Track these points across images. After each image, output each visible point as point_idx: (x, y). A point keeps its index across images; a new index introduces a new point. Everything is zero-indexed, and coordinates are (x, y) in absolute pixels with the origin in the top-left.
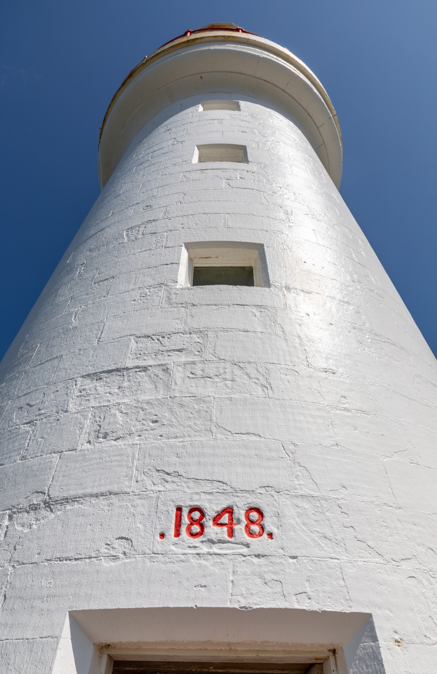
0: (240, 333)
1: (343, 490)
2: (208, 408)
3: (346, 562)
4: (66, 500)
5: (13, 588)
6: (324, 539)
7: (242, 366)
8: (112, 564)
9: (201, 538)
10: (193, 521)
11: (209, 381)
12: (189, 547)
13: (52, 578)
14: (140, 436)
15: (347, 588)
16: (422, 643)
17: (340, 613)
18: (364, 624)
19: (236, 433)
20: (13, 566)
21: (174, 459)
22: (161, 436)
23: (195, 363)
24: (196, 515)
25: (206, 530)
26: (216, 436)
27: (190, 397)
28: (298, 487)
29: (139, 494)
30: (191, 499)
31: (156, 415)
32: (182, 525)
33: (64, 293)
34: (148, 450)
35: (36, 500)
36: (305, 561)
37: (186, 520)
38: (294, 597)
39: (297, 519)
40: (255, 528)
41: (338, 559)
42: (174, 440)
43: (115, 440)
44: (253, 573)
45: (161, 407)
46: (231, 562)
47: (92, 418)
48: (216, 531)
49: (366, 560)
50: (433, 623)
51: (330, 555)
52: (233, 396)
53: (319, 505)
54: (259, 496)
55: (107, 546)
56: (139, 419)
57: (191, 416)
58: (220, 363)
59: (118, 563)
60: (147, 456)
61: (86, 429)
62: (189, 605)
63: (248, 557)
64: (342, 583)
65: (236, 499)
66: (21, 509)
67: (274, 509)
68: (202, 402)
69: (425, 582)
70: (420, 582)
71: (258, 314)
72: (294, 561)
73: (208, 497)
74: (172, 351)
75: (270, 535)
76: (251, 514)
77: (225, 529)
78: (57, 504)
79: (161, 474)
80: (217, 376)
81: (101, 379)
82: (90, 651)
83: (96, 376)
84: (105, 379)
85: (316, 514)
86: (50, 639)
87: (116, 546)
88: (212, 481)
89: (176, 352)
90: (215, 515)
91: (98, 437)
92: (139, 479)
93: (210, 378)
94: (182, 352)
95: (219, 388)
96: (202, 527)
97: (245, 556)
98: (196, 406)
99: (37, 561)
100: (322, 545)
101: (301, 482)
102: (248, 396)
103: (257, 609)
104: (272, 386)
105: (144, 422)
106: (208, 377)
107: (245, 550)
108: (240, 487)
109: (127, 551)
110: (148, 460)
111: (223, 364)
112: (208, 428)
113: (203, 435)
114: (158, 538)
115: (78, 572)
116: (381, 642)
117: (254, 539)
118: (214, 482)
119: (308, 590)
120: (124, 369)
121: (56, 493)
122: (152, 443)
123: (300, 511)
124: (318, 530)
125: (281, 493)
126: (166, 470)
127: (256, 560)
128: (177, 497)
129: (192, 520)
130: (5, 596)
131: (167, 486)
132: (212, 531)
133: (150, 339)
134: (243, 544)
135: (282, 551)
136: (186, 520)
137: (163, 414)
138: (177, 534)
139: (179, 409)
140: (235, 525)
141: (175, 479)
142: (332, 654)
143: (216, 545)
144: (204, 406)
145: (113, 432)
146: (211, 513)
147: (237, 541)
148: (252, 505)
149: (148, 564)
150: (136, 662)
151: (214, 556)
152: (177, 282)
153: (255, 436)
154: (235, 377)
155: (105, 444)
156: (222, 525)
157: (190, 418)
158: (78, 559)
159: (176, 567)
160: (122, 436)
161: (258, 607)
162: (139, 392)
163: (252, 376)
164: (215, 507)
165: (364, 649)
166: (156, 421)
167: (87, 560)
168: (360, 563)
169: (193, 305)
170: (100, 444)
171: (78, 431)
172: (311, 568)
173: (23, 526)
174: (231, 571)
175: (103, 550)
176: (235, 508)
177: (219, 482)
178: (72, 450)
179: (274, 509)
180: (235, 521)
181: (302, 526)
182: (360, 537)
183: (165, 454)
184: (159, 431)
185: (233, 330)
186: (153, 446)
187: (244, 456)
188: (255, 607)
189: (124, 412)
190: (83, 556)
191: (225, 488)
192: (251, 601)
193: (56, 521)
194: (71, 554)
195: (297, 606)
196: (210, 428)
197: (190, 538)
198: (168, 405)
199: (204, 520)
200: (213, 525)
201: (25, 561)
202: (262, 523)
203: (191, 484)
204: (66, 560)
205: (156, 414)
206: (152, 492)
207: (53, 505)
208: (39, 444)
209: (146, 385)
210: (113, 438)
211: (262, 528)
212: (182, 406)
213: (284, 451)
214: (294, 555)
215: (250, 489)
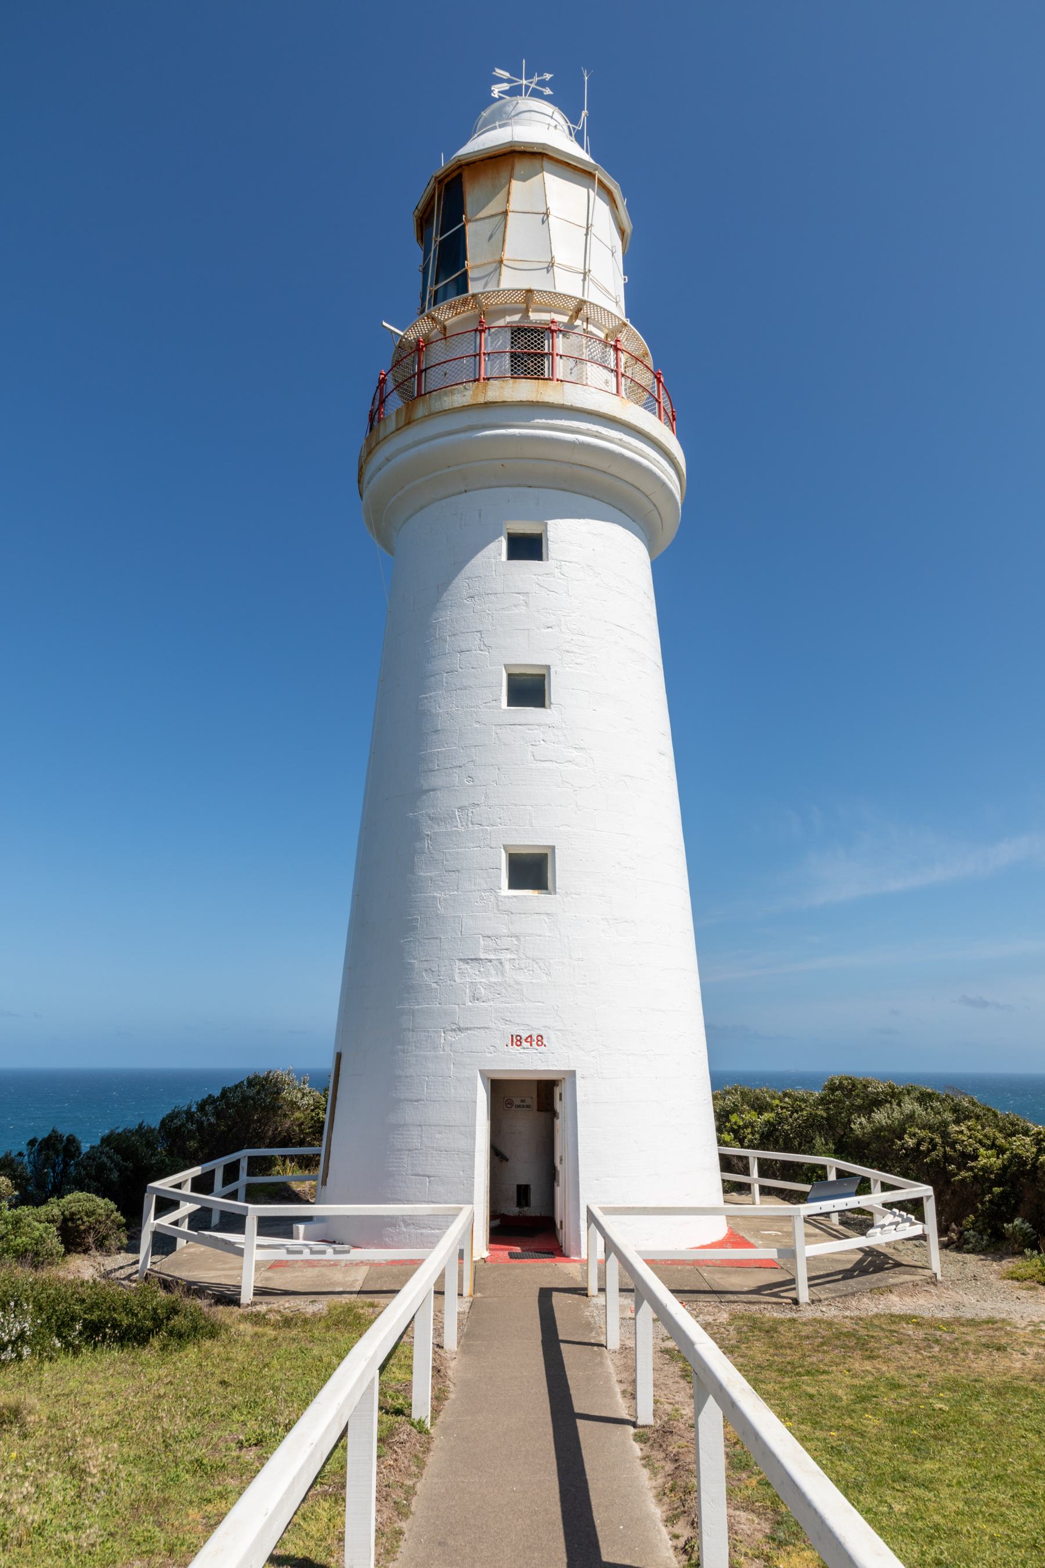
4: (467, 1029)
18: (573, 1073)
35: (454, 1027)
83: (465, 961)
121: (461, 1025)
129: (517, 1040)
132: (524, 1044)
144: (519, 987)
146: (524, 1037)
150: (660, 1278)
155: (477, 1004)
184: (503, 999)
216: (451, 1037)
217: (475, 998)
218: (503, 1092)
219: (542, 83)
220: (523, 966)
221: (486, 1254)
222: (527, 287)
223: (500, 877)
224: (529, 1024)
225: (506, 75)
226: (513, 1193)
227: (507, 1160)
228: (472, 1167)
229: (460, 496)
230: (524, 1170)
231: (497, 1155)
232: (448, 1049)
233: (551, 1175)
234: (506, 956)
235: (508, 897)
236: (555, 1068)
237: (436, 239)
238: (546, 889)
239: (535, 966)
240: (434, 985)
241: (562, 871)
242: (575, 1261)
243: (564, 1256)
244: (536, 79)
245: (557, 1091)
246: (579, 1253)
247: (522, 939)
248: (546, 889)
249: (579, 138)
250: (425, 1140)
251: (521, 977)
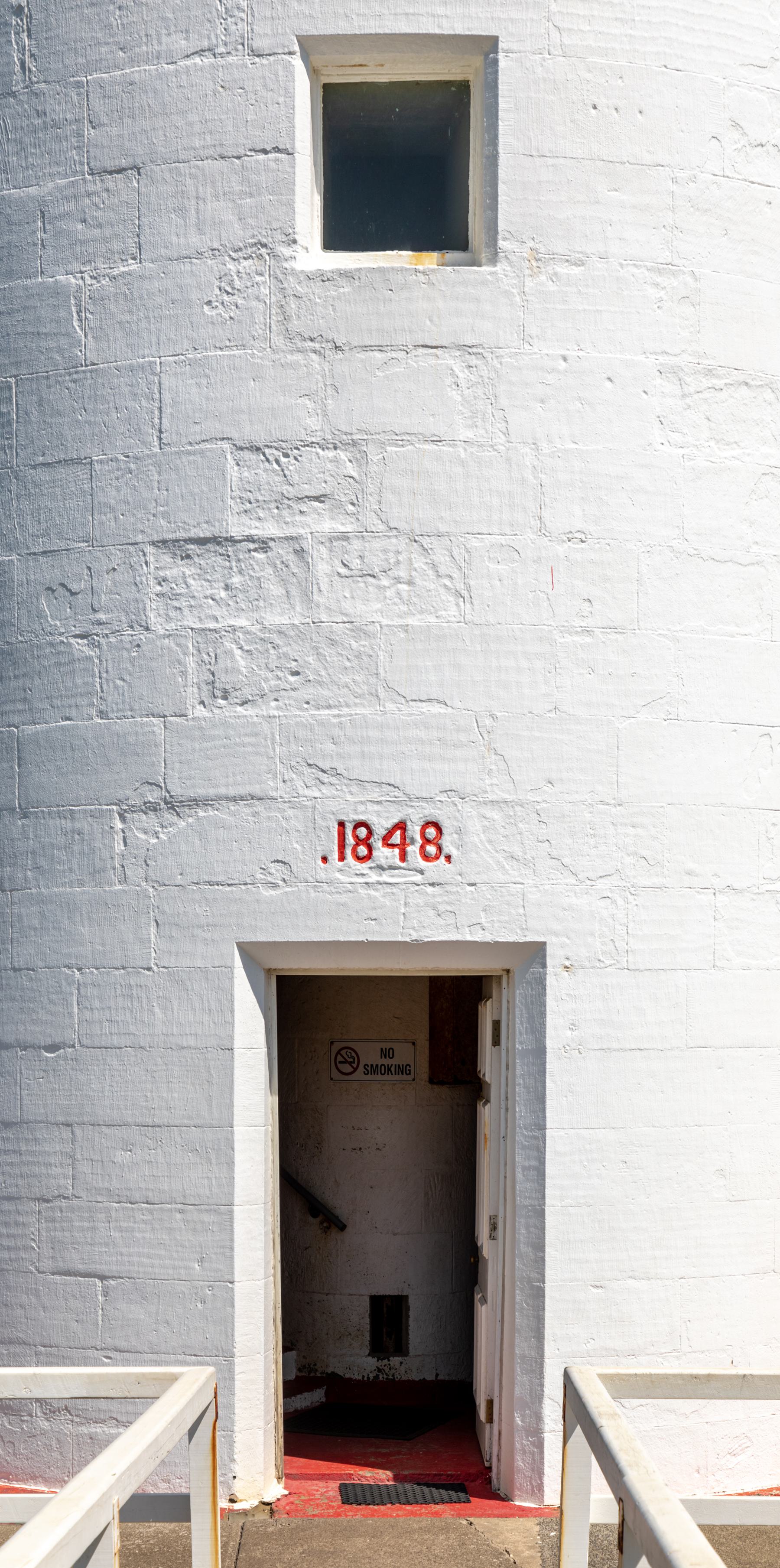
0: (426, 446)
1: (548, 788)
2: (373, 649)
3: (531, 887)
4: (195, 802)
5: (163, 913)
6: (510, 859)
7: (426, 546)
8: (272, 892)
9: (370, 864)
10: (359, 841)
11: (372, 585)
12: (357, 874)
13: (207, 905)
14: (276, 700)
15: (525, 916)
16: (592, 967)
17: (514, 943)
19: (412, 700)
20: (153, 887)
21: (330, 747)
22: (308, 703)
23: (348, 538)
24: (362, 832)
25: (375, 853)
26: (384, 707)
27: (344, 623)
28: (488, 788)
29: (290, 802)
30: (355, 811)
31: (296, 660)
32: (347, 847)
33: (481, 1253)
34: (292, 729)
35: (153, 796)
36: (484, 889)
37: (350, 840)
38: (467, 929)
39: (482, 835)
40: (431, 849)
41: (522, 884)
42: (327, 712)
43: (242, 705)
44: (427, 905)
45: (301, 643)
46: (403, 893)
47: (195, 652)
48: (386, 854)
49: (555, 882)
50: (613, 947)
51: (513, 880)
52: (410, 621)
53: (512, 814)
54: (439, 805)
55: (262, 871)
56: (270, 666)
57: (348, 664)
58: (389, 537)
59: (279, 892)
60: (292, 739)
61: (192, 678)
62: (360, 939)
63: (422, 887)
64: (521, 911)
65: (411, 810)
66: (133, 806)
67: (455, 824)
68: (362, 635)
69: (620, 902)
70: (614, 902)
71: (463, 375)
72: (472, 888)
73: (376, 808)
74: (306, 500)
75: (448, 858)
76: (427, 830)
77: (397, 851)
78: (183, 806)
79: (314, 771)
80: (385, 572)
81: (188, 557)
82: (262, 975)
84: (196, 559)
85: (507, 826)
86: (223, 969)
87: (273, 871)
88: (380, 784)
89: (313, 503)
90: (385, 833)
91: (215, 697)
92: (286, 778)
93: (374, 577)
94: (323, 502)
95: (388, 601)
96: (370, 848)
97: (418, 885)
98: (354, 645)
99: (182, 883)
100: (507, 867)
101: (495, 781)
102: (432, 619)
103: (428, 942)
104: (472, 595)
105: (279, 673)
106: (370, 575)
107: (418, 878)
108: (415, 792)
109: (287, 878)
110: (294, 747)
111: (394, 540)
112: (374, 691)
113: (366, 703)
114: (320, 862)
115: (236, 900)
116: (549, 969)
117: (429, 864)
118: (384, 785)
119: (483, 920)
120: (226, 539)
121: (177, 790)
122: (296, 716)
123: (487, 824)
124: (506, 848)
125: (467, 799)
126: (321, 765)
127: (430, 889)
128: (338, 808)
129: (356, 840)
130: (156, 921)
131: (325, 790)
132: (383, 854)
133: (262, 457)
134: (416, 871)
135: (459, 877)
136: (350, 840)
137: (306, 658)
138: (342, 858)
139: (329, 650)
140: (408, 845)
141: (333, 780)
142: (505, 973)
143: (387, 872)
145: (236, 690)
146: (380, 831)
147: (410, 867)
148: (429, 819)
149: (313, 894)
151: (385, 886)
152: (295, 242)
153: (439, 705)
154: (414, 573)
156: (393, 846)
157: (346, 668)
158: (232, 885)
159: (343, 898)
160: (251, 698)
161: (429, 940)
162: (262, 604)
163: (443, 570)
164: (384, 823)
165: (533, 973)
166: (297, 673)
167: (243, 887)
168: (546, 887)
169: (336, 347)
170: (221, 710)
171: (180, 679)
172: (489, 897)
173: (146, 833)
174: (402, 902)
175: (259, 876)
176: (409, 823)
177: (390, 785)
178: (180, 716)
179: (455, 824)
180: (408, 841)
181: (487, 845)
182: (554, 853)
183: (316, 737)
184: (307, 693)
185: (413, 437)
186: (298, 722)
187: (422, 742)
188: (426, 940)
189: (246, 648)
190: (237, 882)
191: (396, 794)
192: (423, 934)
193: (190, 831)
194: (221, 878)
195: (469, 938)
196: (377, 691)
197: (357, 863)
198: (311, 639)
199: (372, 840)
200: (383, 846)
201: (167, 883)
202: (440, 842)
203: (355, 789)
204: (218, 885)
205: (296, 658)
206: (305, 799)
207: (178, 806)
208: (121, 691)
209: (272, 587)
210: (238, 701)
211: (440, 849)
212: (333, 642)
213: (477, 729)
214: (473, 881)
215: (428, 796)
216: (146, 832)
217: (218, 691)
218: (316, 1016)
220: (376, 562)
221: (275, 1491)
223: (290, 185)
224: (406, 780)
226: (359, 1315)
227: (342, 1227)
228: (228, 1250)
230: (385, 1253)
231: (306, 1208)
232: (135, 873)
233: (463, 1271)
234: (322, 523)
235: (323, 278)
236: (478, 936)
238: (462, 244)
239: (419, 563)
240: (80, 646)
241: (523, 161)
242: (524, 1512)
243: (494, 1496)
245: (487, 1014)
246: (538, 1490)
247: (374, 456)
248: (462, 244)
250: (84, 1168)
251: (368, 606)
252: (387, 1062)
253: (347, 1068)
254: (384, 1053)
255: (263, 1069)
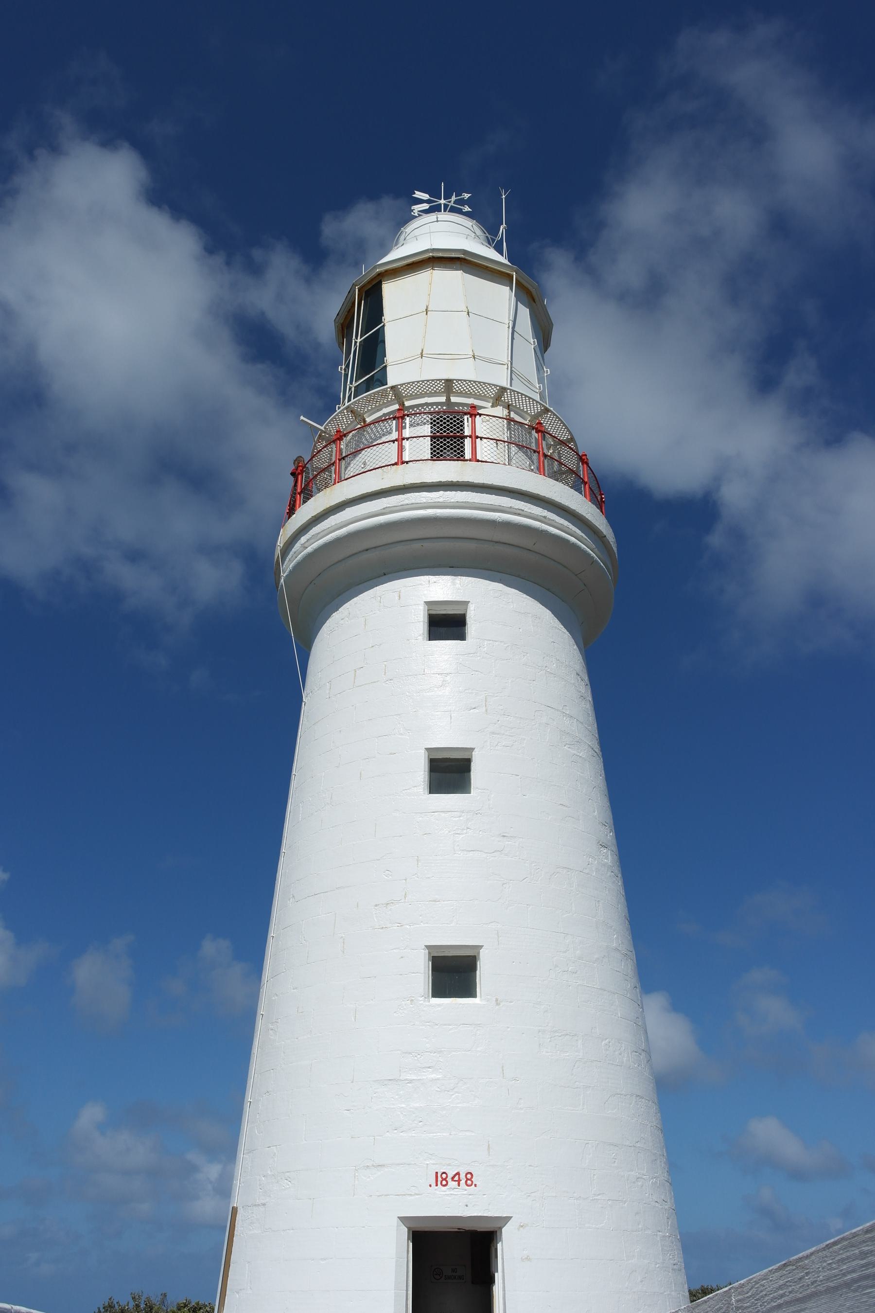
10: (443, 1179)
24: (444, 1176)
37: (440, 1179)
40: (469, 1182)
129: (441, 1179)
132: (452, 1184)
146: (450, 1175)
219: (462, 202)
222: (446, 377)
225: (425, 196)
229: (488, 436)
237: (358, 340)
244: (454, 198)
249: (499, 249)
252: (454, 1274)
253: (438, 1277)
254: (453, 1271)
255: (422, 628)
